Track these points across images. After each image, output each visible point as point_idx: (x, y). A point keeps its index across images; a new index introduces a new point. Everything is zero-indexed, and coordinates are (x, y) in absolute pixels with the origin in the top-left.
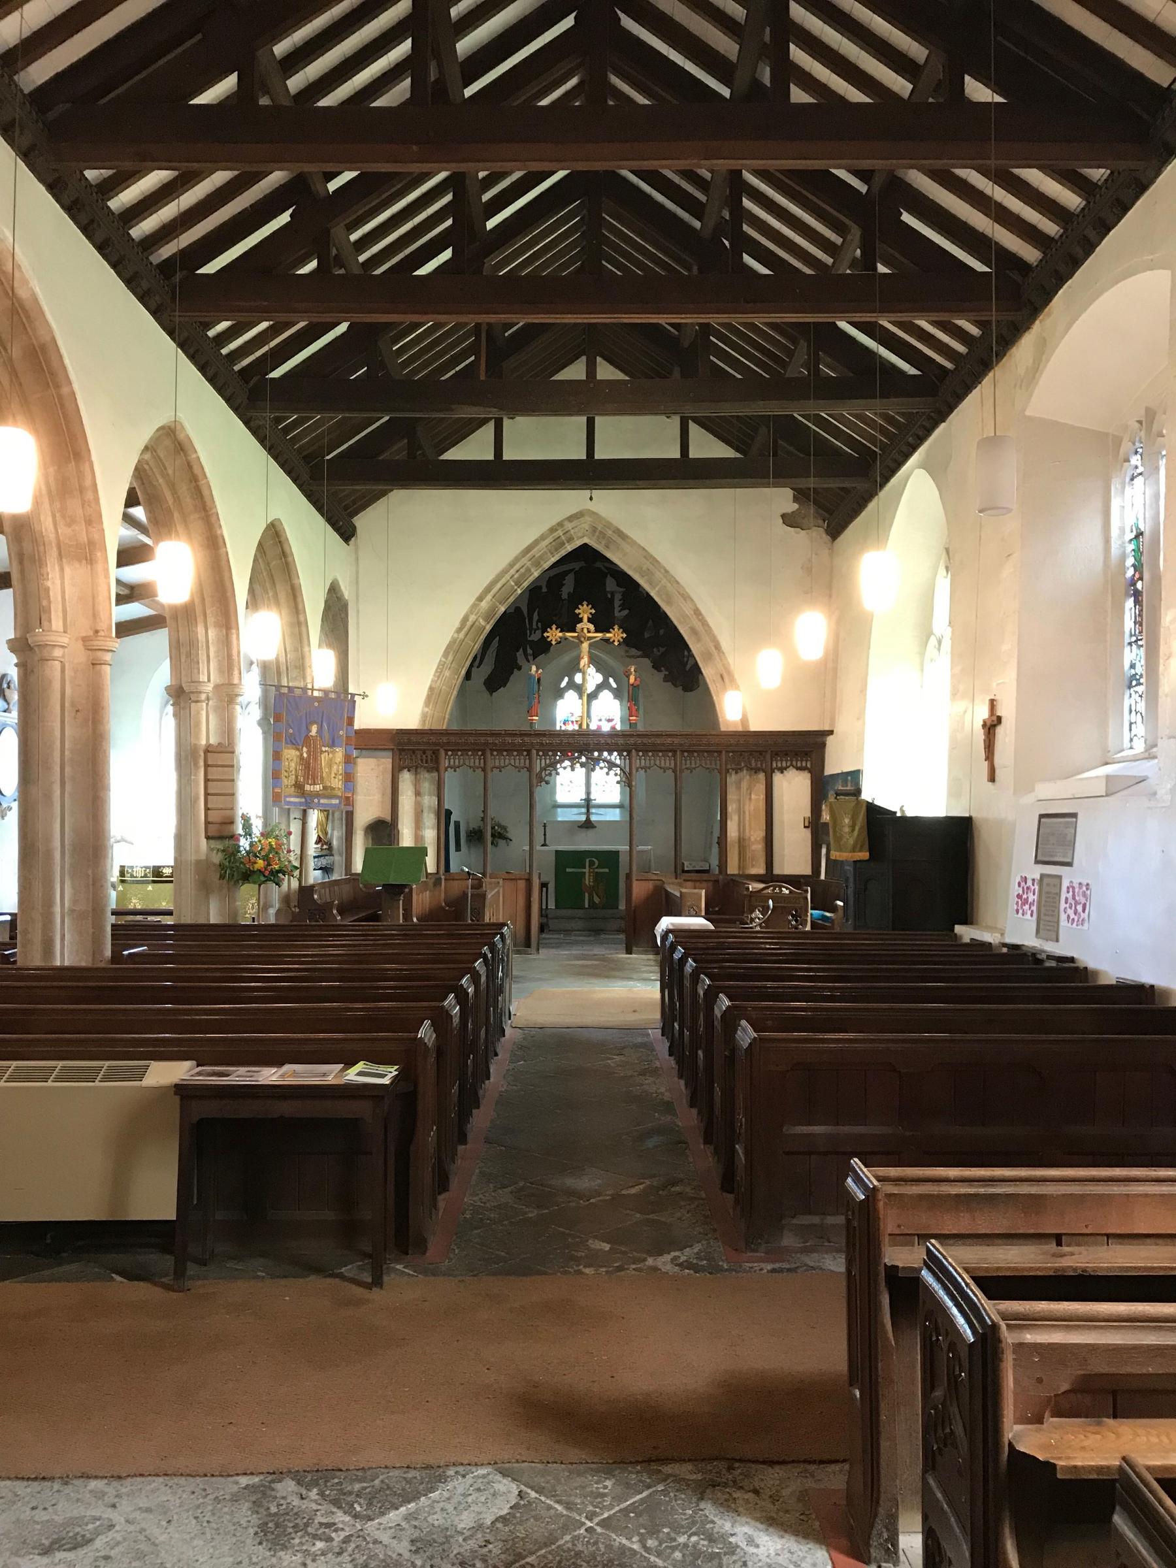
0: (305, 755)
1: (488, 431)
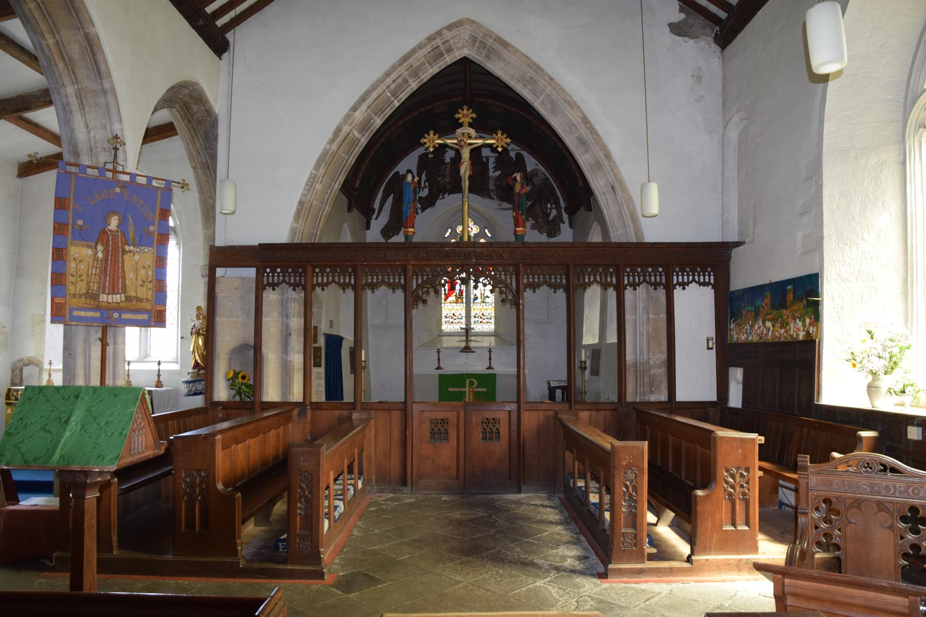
0: (100, 255)
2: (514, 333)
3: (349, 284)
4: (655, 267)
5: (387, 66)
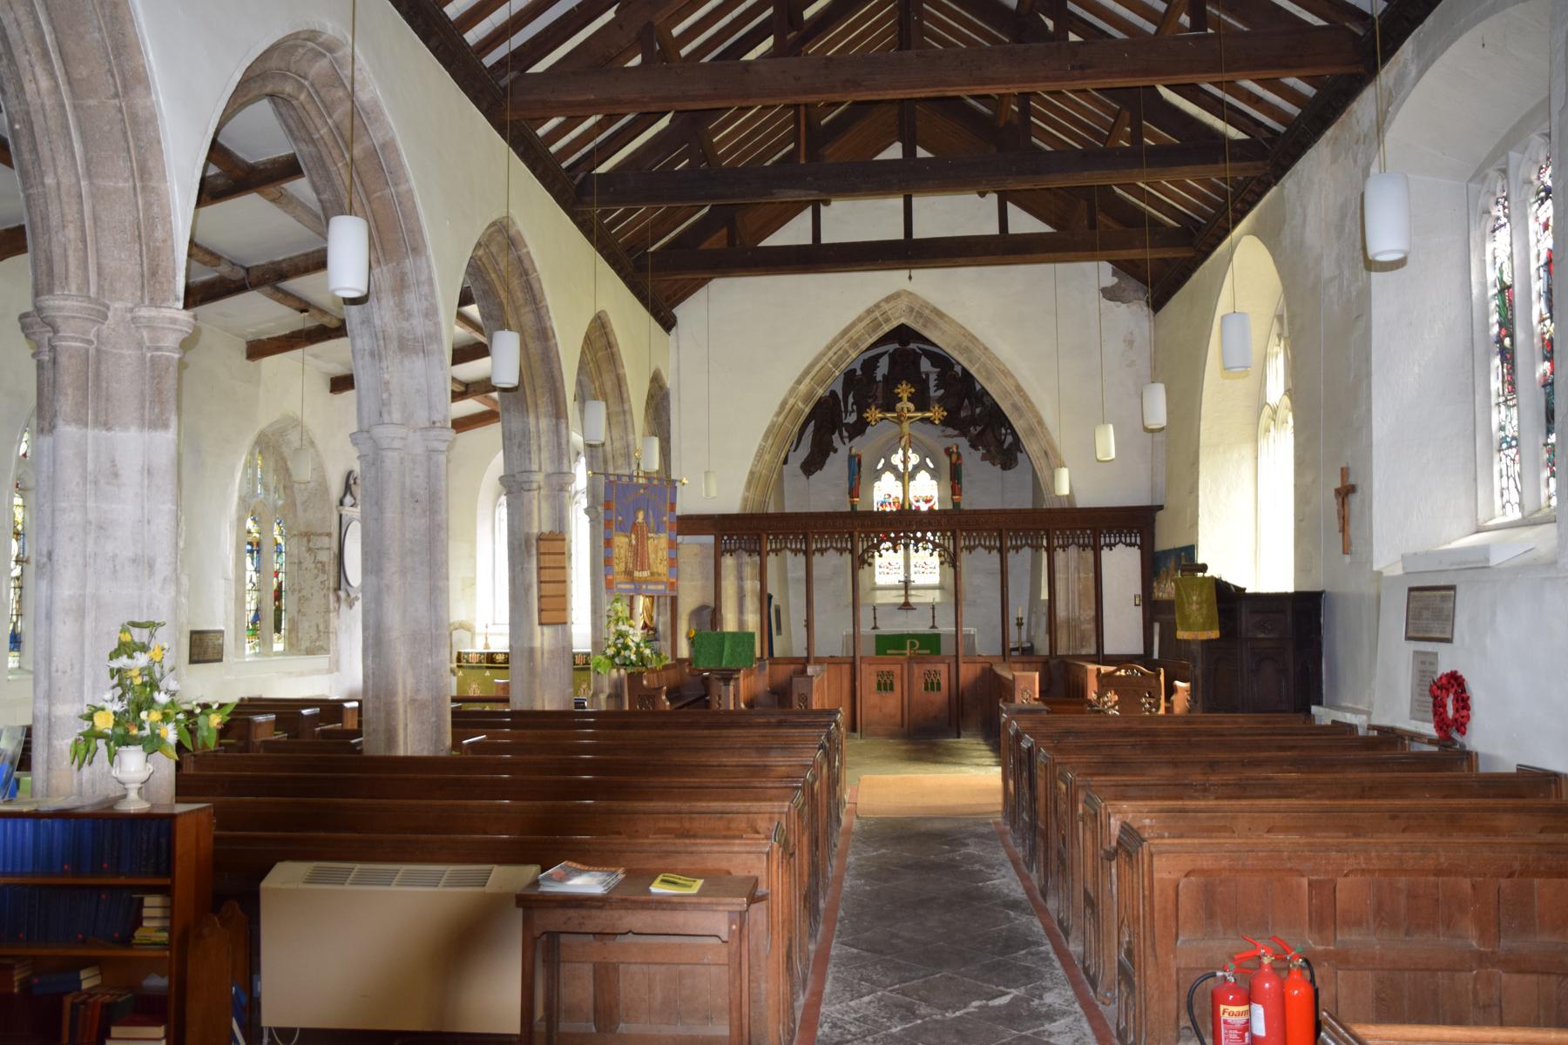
1: (807, 215)
2: (955, 591)
4: (1083, 529)
5: (829, 340)
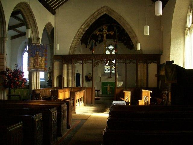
0: (35, 59)
3: (81, 63)
